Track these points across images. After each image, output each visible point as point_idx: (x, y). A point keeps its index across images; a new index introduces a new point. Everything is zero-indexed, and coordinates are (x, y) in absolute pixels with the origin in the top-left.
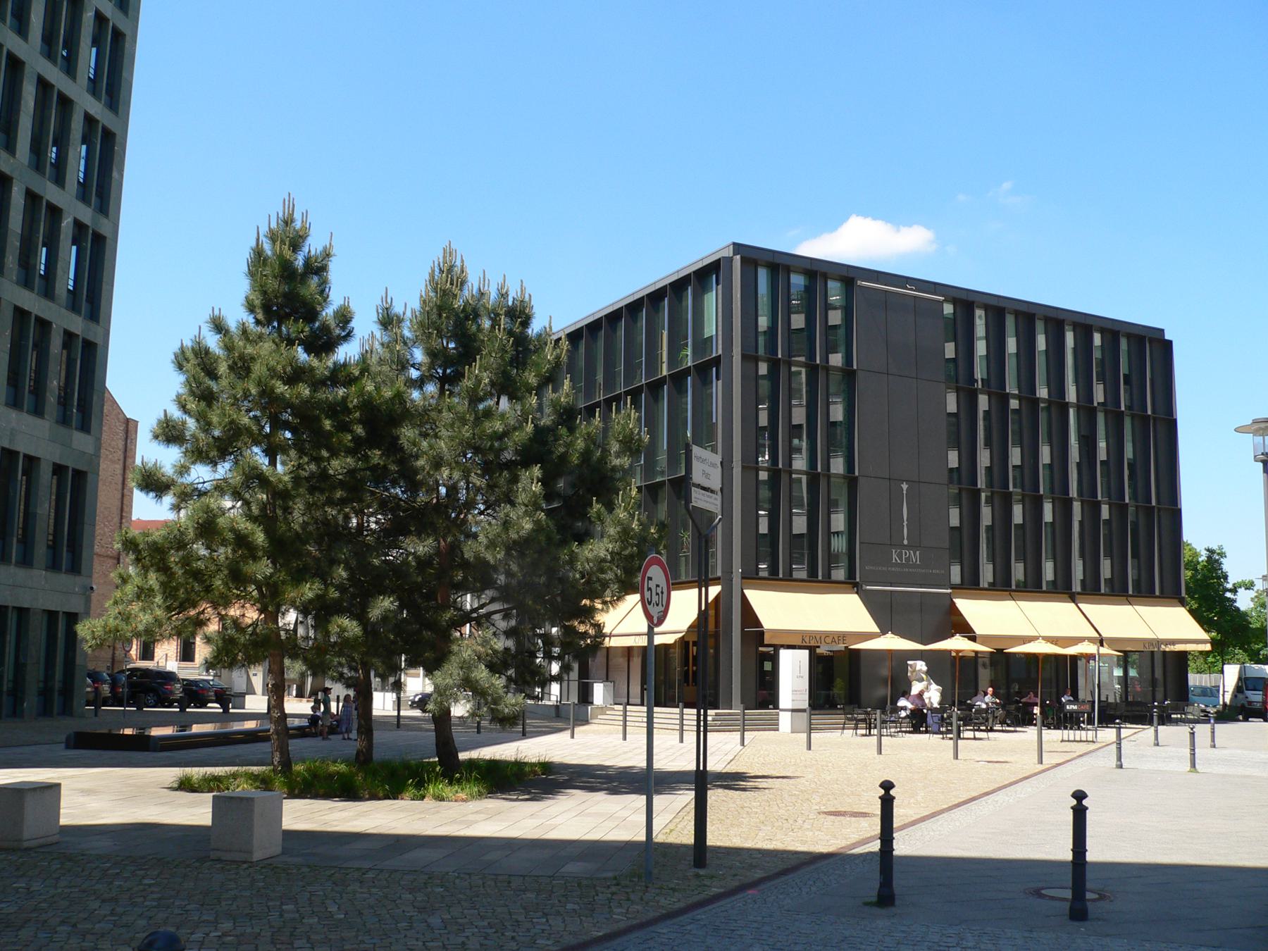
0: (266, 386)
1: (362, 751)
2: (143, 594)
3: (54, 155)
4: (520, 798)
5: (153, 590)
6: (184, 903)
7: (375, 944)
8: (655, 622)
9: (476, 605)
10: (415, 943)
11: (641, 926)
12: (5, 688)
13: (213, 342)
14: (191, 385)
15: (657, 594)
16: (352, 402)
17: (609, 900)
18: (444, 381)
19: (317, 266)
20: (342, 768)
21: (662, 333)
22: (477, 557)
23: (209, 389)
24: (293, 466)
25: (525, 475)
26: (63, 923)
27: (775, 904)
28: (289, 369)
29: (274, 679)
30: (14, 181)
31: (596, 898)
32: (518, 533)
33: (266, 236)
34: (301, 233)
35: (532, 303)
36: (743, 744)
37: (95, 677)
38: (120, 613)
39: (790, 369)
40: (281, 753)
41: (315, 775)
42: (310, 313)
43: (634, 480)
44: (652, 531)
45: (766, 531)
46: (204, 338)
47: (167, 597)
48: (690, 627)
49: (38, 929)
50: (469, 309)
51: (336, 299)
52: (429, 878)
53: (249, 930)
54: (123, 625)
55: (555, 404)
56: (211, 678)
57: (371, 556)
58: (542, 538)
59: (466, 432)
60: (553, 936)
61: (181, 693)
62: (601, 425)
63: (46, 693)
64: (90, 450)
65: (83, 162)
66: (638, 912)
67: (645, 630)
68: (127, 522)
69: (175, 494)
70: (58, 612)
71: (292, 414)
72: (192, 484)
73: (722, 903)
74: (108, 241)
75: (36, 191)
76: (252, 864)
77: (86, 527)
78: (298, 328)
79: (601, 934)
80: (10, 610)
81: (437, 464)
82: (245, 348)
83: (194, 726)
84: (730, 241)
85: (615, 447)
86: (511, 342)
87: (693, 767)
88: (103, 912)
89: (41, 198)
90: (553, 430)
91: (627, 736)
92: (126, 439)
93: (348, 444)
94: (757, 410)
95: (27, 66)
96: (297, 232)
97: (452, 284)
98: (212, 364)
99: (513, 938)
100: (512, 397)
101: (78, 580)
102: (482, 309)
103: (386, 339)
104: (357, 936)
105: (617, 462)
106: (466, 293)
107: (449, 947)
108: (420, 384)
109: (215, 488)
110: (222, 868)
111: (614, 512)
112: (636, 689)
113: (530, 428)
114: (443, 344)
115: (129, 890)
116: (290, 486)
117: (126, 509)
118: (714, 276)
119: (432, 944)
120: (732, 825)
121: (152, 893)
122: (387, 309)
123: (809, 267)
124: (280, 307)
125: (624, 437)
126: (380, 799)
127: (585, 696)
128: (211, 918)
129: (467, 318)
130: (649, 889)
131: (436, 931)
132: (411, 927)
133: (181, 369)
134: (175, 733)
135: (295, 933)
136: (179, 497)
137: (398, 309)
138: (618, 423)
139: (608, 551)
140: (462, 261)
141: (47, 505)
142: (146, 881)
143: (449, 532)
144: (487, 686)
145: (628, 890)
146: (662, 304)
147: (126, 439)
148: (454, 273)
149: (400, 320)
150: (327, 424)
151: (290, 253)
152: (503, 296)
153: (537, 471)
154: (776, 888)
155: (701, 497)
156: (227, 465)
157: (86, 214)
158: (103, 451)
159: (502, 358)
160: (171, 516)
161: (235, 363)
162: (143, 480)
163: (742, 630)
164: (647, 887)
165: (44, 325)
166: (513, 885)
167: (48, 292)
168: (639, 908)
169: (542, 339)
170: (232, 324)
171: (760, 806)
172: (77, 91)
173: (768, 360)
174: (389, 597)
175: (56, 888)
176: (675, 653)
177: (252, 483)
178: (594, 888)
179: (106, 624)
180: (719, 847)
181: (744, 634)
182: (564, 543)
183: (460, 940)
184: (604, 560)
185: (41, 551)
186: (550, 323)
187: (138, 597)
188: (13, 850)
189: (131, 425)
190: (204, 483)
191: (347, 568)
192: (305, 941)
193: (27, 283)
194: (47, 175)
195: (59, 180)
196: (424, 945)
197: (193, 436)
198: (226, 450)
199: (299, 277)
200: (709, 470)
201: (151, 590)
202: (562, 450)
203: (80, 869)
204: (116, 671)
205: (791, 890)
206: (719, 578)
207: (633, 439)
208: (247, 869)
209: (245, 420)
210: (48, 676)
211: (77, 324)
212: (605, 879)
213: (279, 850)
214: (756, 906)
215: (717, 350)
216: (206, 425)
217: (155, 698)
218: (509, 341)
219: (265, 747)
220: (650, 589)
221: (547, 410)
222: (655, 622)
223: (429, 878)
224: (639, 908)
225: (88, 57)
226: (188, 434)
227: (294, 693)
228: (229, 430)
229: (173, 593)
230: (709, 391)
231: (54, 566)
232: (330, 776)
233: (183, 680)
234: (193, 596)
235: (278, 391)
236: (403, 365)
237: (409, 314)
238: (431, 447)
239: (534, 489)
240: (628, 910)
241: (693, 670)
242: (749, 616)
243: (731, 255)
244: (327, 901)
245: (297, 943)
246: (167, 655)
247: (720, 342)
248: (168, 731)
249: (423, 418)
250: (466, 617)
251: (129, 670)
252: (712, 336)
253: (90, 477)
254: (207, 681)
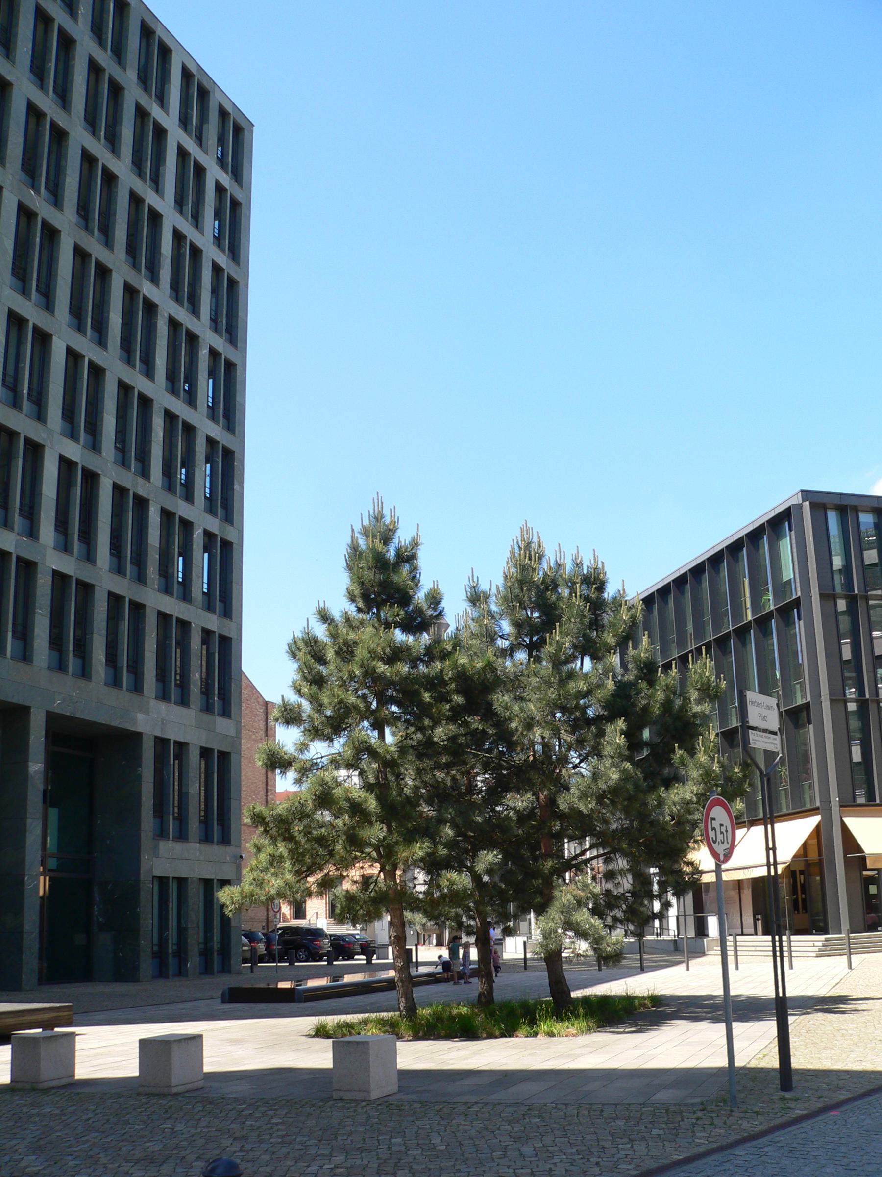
0: (368, 666)
1: (483, 993)
2: (275, 860)
3: (183, 477)
4: (627, 1030)
5: (283, 857)
6: (305, 1139)
7: (469, 1172)
8: (722, 858)
9: (578, 852)
10: (507, 1170)
11: (721, 1149)
12: (170, 951)
13: (320, 631)
14: (303, 672)
15: (722, 833)
16: (447, 674)
17: (694, 1125)
18: (532, 648)
19: (407, 555)
20: (464, 1010)
21: (744, 581)
22: (572, 809)
23: (319, 673)
24: (402, 736)
25: (609, 729)
26: (198, 1159)
27: (855, 1124)
28: (388, 650)
29: (396, 932)
30: (150, 502)
31: (681, 1123)
32: (606, 782)
33: (360, 533)
34: (391, 527)
35: (606, 569)
36: (850, 967)
37: (251, 936)
38: (254, 879)
39: (867, 603)
40: (406, 999)
41: (438, 1018)
42: (403, 598)
43: (711, 725)
44: (737, 770)
45: (860, 760)
46: (312, 628)
47: (294, 862)
48: (795, 857)
49: (177, 1164)
50: (549, 581)
51: (426, 584)
52: (529, 1110)
53: (359, 1162)
54: (257, 890)
55: (636, 660)
56: (358, 932)
57: (474, 814)
58: (630, 786)
59: (552, 694)
60: (635, 1160)
61: (330, 947)
62: (678, 676)
63: (206, 953)
64: (232, 733)
65: (208, 479)
66: (720, 1135)
67: (713, 867)
68: (272, 794)
69: (295, 769)
70: (212, 880)
71: (396, 690)
72: (312, 759)
73: (803, 1124)
74: (234, 546)
75: (170, 509)
76: (369, 1102)
77: (233, 802)
78: (394, 612)
79: (681, 1158)
80: (171, 880)
81: (529, 725)
82: (348, 634)
83: (346, 976)
84: (799, 489)
85: (694, 695)
86: (588, 607)
87: (773, 995)
88: (233, 1149)
89: (174, 514)
90: (634, 685)
91: (739, 965)
93: (447, 713)
94: (840, 645)
95: (155, 402)
96: (387, 526)
97: (530, 559)
98: (321, 651)
99: (597, 1164)
100: (595, 658)
101: (229, 850)
102: (560, 579)
103: (475, 615)
104: (454, 1166)
105: (697, 709)
106: (545, 566)
107: (537, 1173)
108: (510, 652)
109: (331, 762)
110: (343, 1107)
111: (695, 756)
112: (748, 919)
113: (610, 685)
114: (527, 614)
115: (259, 1128)
116: (396, 756)
117: (270, 783)
118: (787, 523)
119: (522, 1171)
120: (825, 1048)
121: (278, 1131)
122: (474, 587)
123: (876, 505)
124: (378, 595)
125: (702, 685)
126: (496, 1037)
127: (701, 930)
128: (327, 1152)
129: (547, 589)
130: (733, 1113)
131: (526, 1159)
132: (505, 1156)
133: (295, 658)
134: (329, 984)
135: (399, 1164)
136: (300, 772)
137: (484, 586)
138: (695, 672)
139: (693, 793)
140: (539, 537)
141: (197, 785)
142: (274, 1121)
143: (545, 786)
144: (587, 926)
145: (714, 1115)
146: (740, 554)
148: (532, 549)
149: (487, 597)
150: (427, 697)
151: (381, 545)
152: (579, 565)
153: (621, 724)
154: (858, 1108)
155: (759, 738)
156: (342, 740)
157: (214, 524)
158: (243, 732)
159: (581, 623)
160: (295, 788)
161: (341, 649)
162: (267, 759)
163: (845, 856)
164: (732, 1111)
165: (184, 625)
166: (605, 1114)
167: (186, 596)
168: (722, 1132)
169: (617, 603)
170: (336, 614)
171: (857, 1028)
172: (199, 418)
173: (846, 597)
174: (493, 851)
175: (196, 1127)
176: (783, 883)
177: (363, 755)
178: (681, 1114)
179: (242, 890)
180: (809, 1070)
181: (847, 861)
182: (653, 788)
183: (548, 1166)
184: (690, 802)
185: (194, 825)
186: (623, 586)
187: (272, 864)
188: (163, 1095)
190: (322, 757)
191: (454, 826)
192: (407, 1171)
193: (167, 590)
194: (178, 495)
195: (189, 497)
196: (514, 1172)
197: (309, 716)
198: (339, 726)
199: (391, 567)
200: (765, 712)
201: (281, 857)
202: (644, 702)
203: (218, 1111)
204: (270, 930)
205: (874, 1111)
206: (818, 809)
207: (710, 686)
208: (365, 1106)
209: (353, 699)
210: (208, 939)
211: (213, 622)
212: (692, 1104)
213: (395, 1088)
214: (837, 1127)
215: (796, 593)
216: (319, 707)
217: (306, 953)
218: (586, 607)
219: (393, 994)
220: (713, 829)
221: (631, 666)
222: (722, 858)
223: (529, 1110)
224: (722, 1132)
225: (206, 388)
226: (304, 715)
227: (434, 942)
228: (339, 709)
229: (300, 858)
230: (792, 632)
231: (207, 838)
232: (452, 1018)
233: (331, 936)
234: (318, 860)
235: (379, 671)
236: (491, 637)
237: (494, 590)
238: (522, 710)
239: (618, 741)
240: (710, 1134)
241: (802, 899)
242: (850, 843)
243: (801, 502)
244: (433, 1134)
245: (400, 1173)
246: (317, 913)
247: (798, 584)
248: (322, 982)
249: (514, 683)
250: (568, 865)
251: (280, 929)
252: (790, 579)
253: (233, 757)
254: (353, 936)
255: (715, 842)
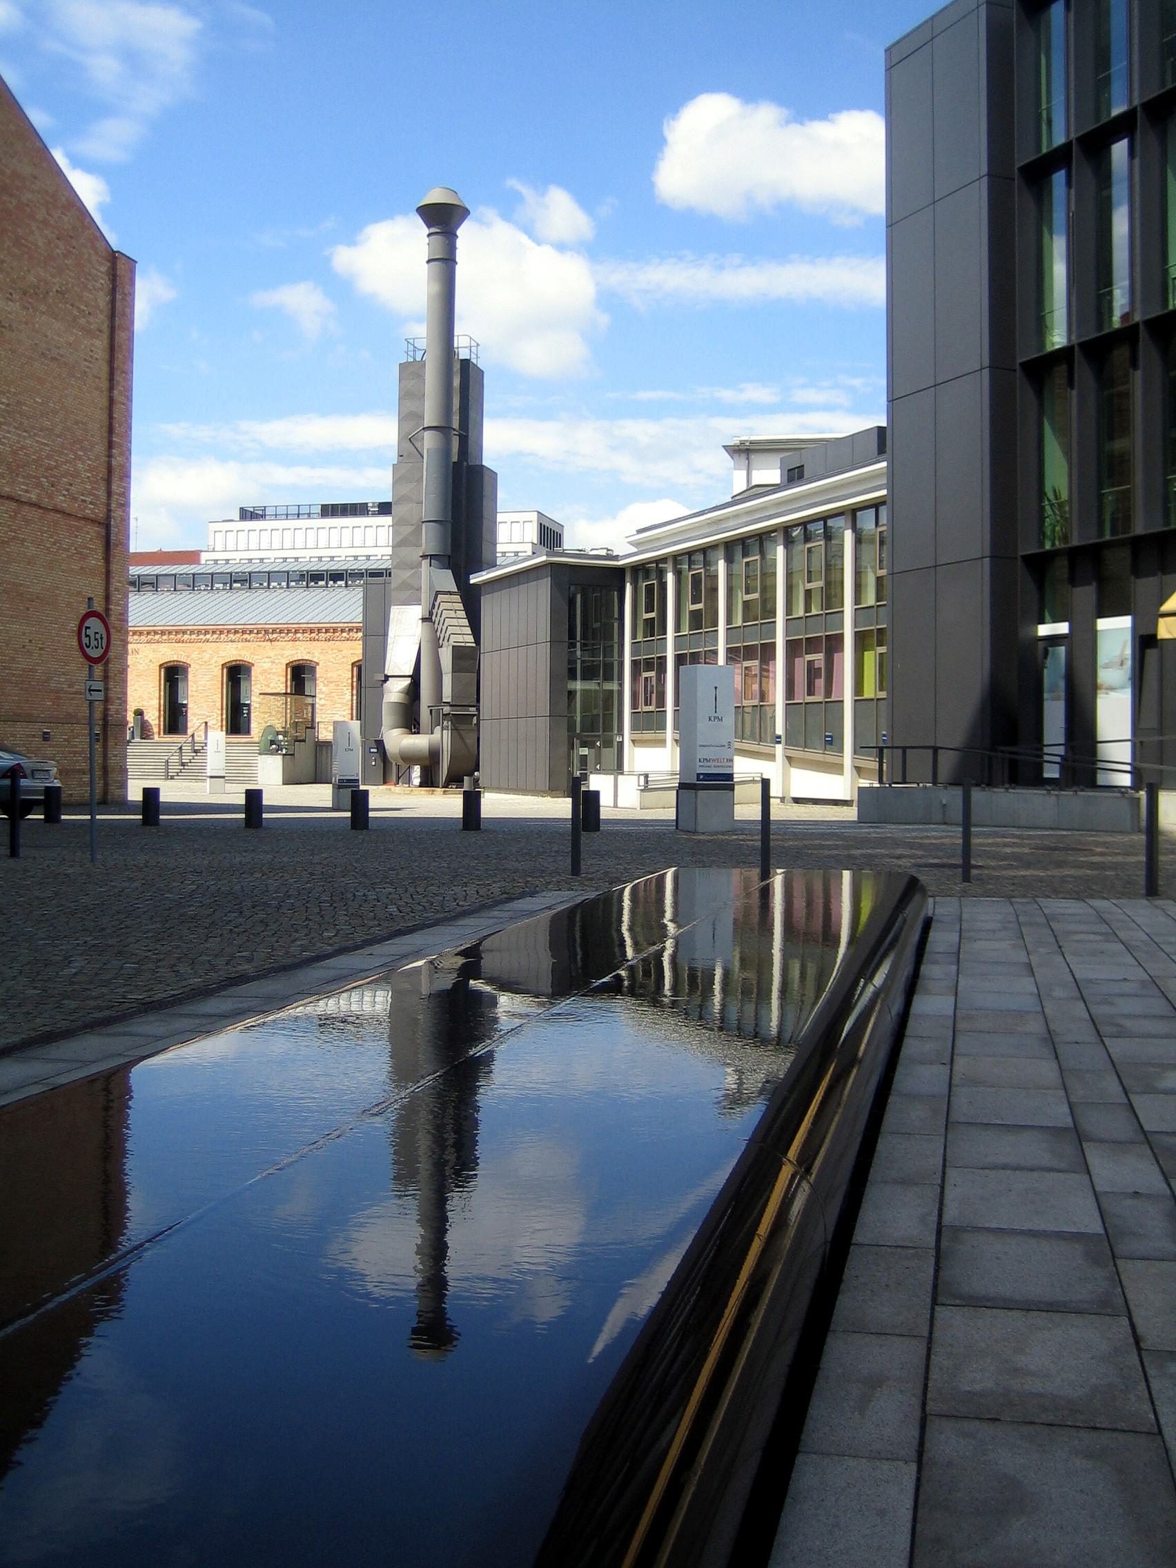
92: (113, 291)
147: (113, 291)
189: (121, 266)
227: (417, 781)
255: (88, 647)
